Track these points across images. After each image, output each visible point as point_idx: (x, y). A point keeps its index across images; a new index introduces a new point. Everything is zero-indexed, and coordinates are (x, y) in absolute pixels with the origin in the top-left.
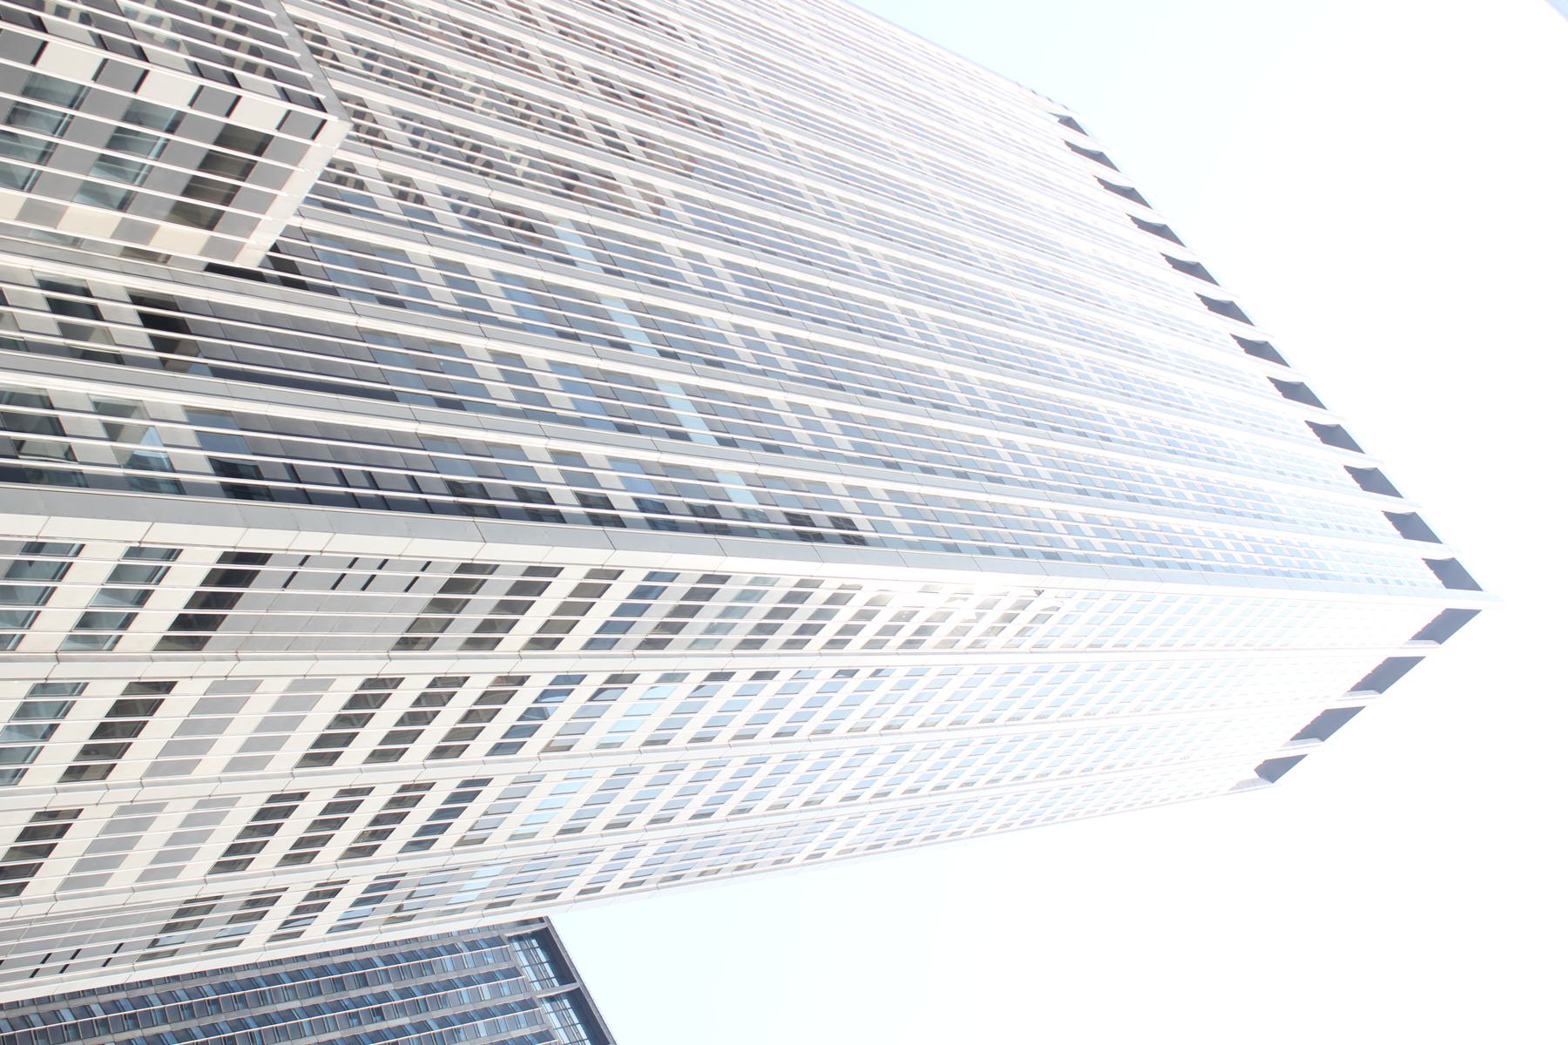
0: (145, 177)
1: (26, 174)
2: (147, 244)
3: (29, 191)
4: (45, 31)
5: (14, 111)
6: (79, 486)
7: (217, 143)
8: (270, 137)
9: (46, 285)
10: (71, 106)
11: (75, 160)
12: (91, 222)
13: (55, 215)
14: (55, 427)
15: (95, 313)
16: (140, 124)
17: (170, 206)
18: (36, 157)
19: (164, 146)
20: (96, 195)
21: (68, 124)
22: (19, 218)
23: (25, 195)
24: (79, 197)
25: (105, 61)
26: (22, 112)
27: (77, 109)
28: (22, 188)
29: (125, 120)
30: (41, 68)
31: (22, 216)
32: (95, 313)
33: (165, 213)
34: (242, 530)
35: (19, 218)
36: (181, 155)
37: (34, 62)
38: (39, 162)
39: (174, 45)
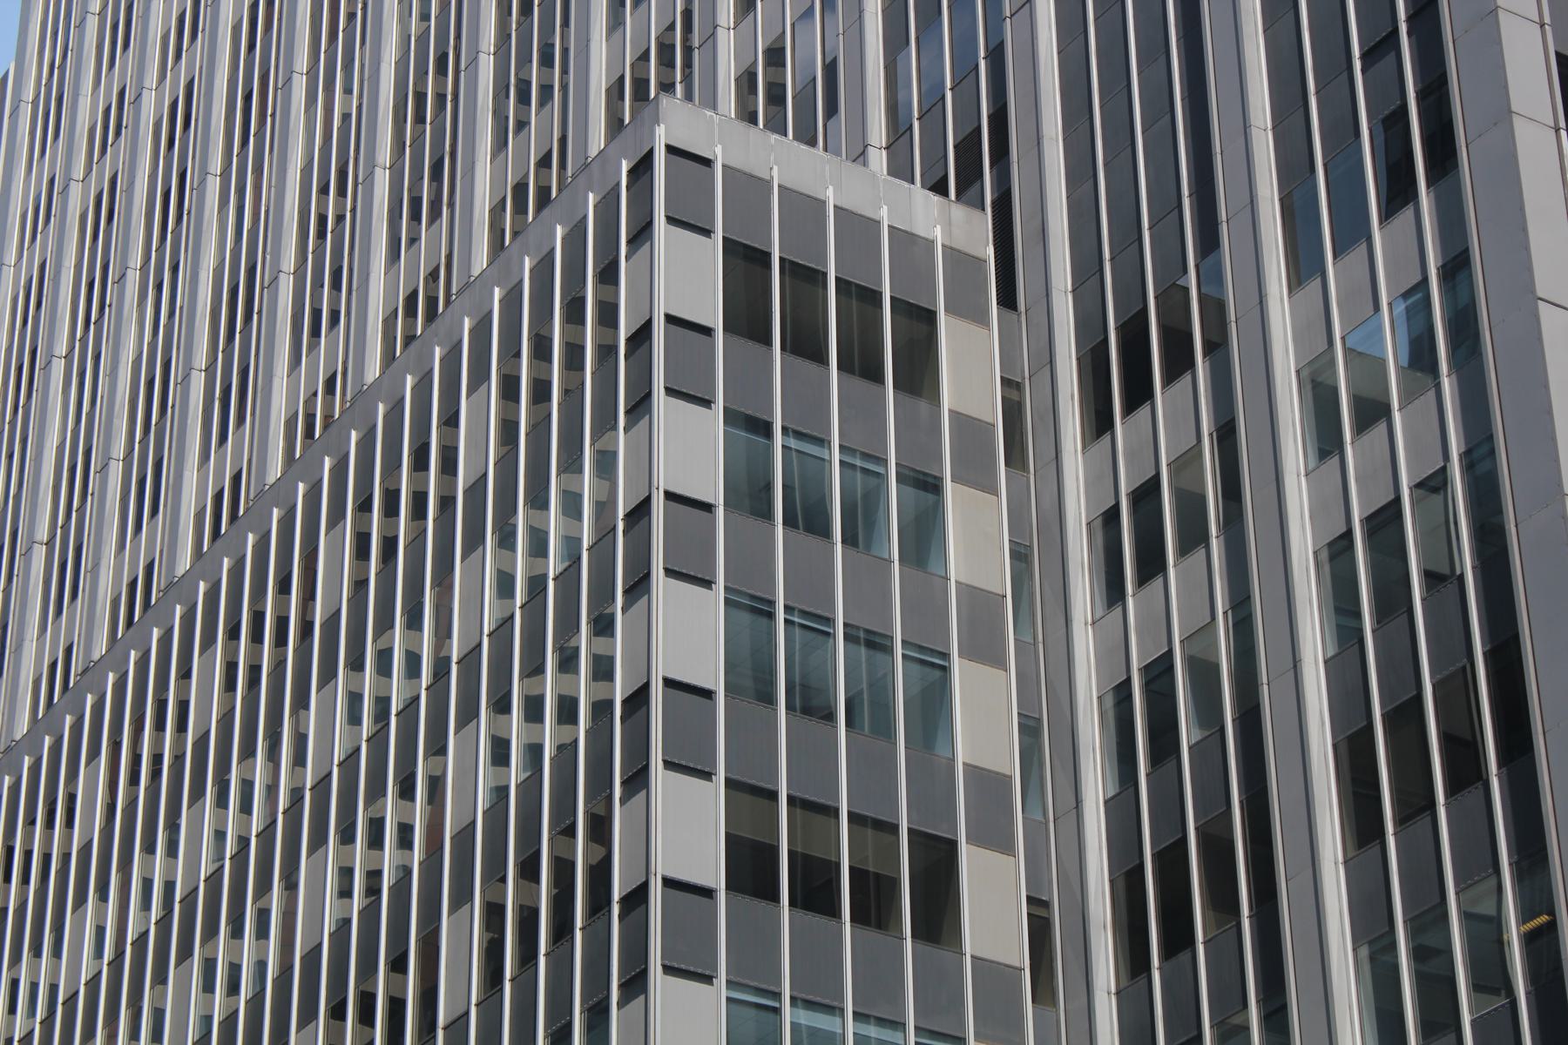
0: (881, 1022)
1: (916, 667)
2: (1008, 779)
3: (946, 656)
4: (644, 690)
5: (807, 711)
6: (1492, 452)
8: (729, 783)
9: (1114, 592)
10: (771, 616)
11: (867, 586)
13: (979, 603)
14: (1385, 521)
15: (1146, 495)
17: (908, 400)
20: (924, 537)
21: (804, 614)
22: (1001, 664)
23: (957, 664)
24: (933, 566)
26: (806, 697)
27: (772, 603)
28: (945, 670)
29: (768, 515)
30: (717, 878)
32: (1146, 495)
33: (941, 954)
34: (1518, 123)
35: (1001, 664)
39: (605, 464)
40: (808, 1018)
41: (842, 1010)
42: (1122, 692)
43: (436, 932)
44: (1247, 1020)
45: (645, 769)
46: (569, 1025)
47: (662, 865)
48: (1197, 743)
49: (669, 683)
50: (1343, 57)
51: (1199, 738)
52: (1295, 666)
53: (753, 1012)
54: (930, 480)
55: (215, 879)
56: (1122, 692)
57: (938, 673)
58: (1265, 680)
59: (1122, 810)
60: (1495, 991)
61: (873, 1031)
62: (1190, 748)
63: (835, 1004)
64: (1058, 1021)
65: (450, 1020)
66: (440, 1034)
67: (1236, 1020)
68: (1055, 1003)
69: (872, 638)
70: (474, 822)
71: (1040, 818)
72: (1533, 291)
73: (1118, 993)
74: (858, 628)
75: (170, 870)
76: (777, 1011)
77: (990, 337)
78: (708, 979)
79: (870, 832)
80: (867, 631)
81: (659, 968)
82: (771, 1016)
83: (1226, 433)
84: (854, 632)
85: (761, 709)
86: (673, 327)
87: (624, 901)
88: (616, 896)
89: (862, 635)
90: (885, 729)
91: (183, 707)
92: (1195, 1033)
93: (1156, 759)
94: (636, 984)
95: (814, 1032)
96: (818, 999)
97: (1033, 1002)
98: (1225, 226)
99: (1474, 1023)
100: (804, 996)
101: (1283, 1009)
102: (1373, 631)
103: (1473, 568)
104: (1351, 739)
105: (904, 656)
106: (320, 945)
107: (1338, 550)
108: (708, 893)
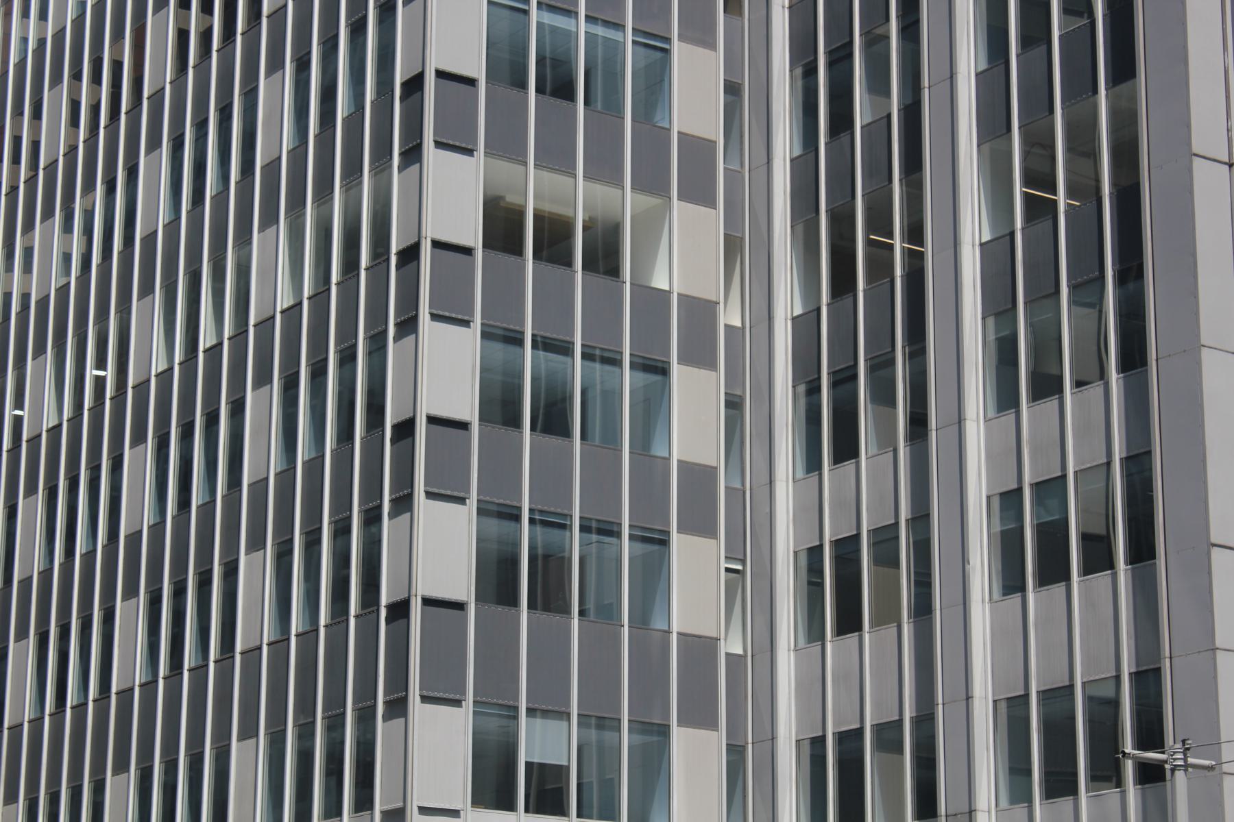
0: (607, 23)
1: (642, 50)
2: (714, 143)
3: (668, 40)
7: (518, 251)
12: (693, 422)
13: (698, 478)
16: (514, 562)
18: (608, 735)
19: (552, 9)
21: (541, 512)
23: (676, 47)
25: (435, 317)
26: (548, 414)
27: (520, 509)
28: (666, 52)
29: (523, 85)
30: (476, 67)
31: (709, 531)
34: (1210, 362)
36: (554, 302)
37: (471, 82)
38: (618, 535)
40: (550, 19)
41: (576, 13)
42: (815, 553)
43: (255, 90)
44: (888, 31)
45: (410, 497)
46: (365, 18)
47: (432, 230)
48: (869, 124)
49: (440, 74)
50: (1046, 87)
51: (870, 120)
52: (952, 77)
53: (507, 13)
54: (660, 365)
55: (63, 291)
56: (815, 553)
57: (659, 55)
58: (940, 701)
59: (804, 170)
60: (1079, 14)
61: (600, 31)
62: (862, 127)
63: (572, 8)
64: (744, 200)
65: (273, 9)
66: (264, 21)
67: (879, 31)
68: (741, 14)
69: (606, 354)
70: (279, 158)
71: (738, 486)
72: (1189, 144)
73: (790, 7)
74: (591, 519)
75: (26, 282)
76: (526, 12)
77: (717, 59)
78: (469, 152)
79: (598, 366)
80: (598, 521)
81: (432, 144)
82: (521, 16)
83: (912, 114)
84: (587, 523)
85: (514, 93)
86: (437, 251)
87: (405, 85)
88: (394, 249)
89: (598, 352)
90: (612, 438)
91: (35, 146)
92: (848, 40)
93: (833, 131)
94: (408, 325)
95: (554, 30)
96: (559, 5)
97: (725, 12)
98: (926, 91)
99: (1061, 37)
100: (539, 507)
101: (916, 23)
102: (1018, 56)
103: (1104, 16)
104: (1004, 534)
105: (634, 42)
106: (156, 232)
107: (1009, 500)
108: (468, 251)
